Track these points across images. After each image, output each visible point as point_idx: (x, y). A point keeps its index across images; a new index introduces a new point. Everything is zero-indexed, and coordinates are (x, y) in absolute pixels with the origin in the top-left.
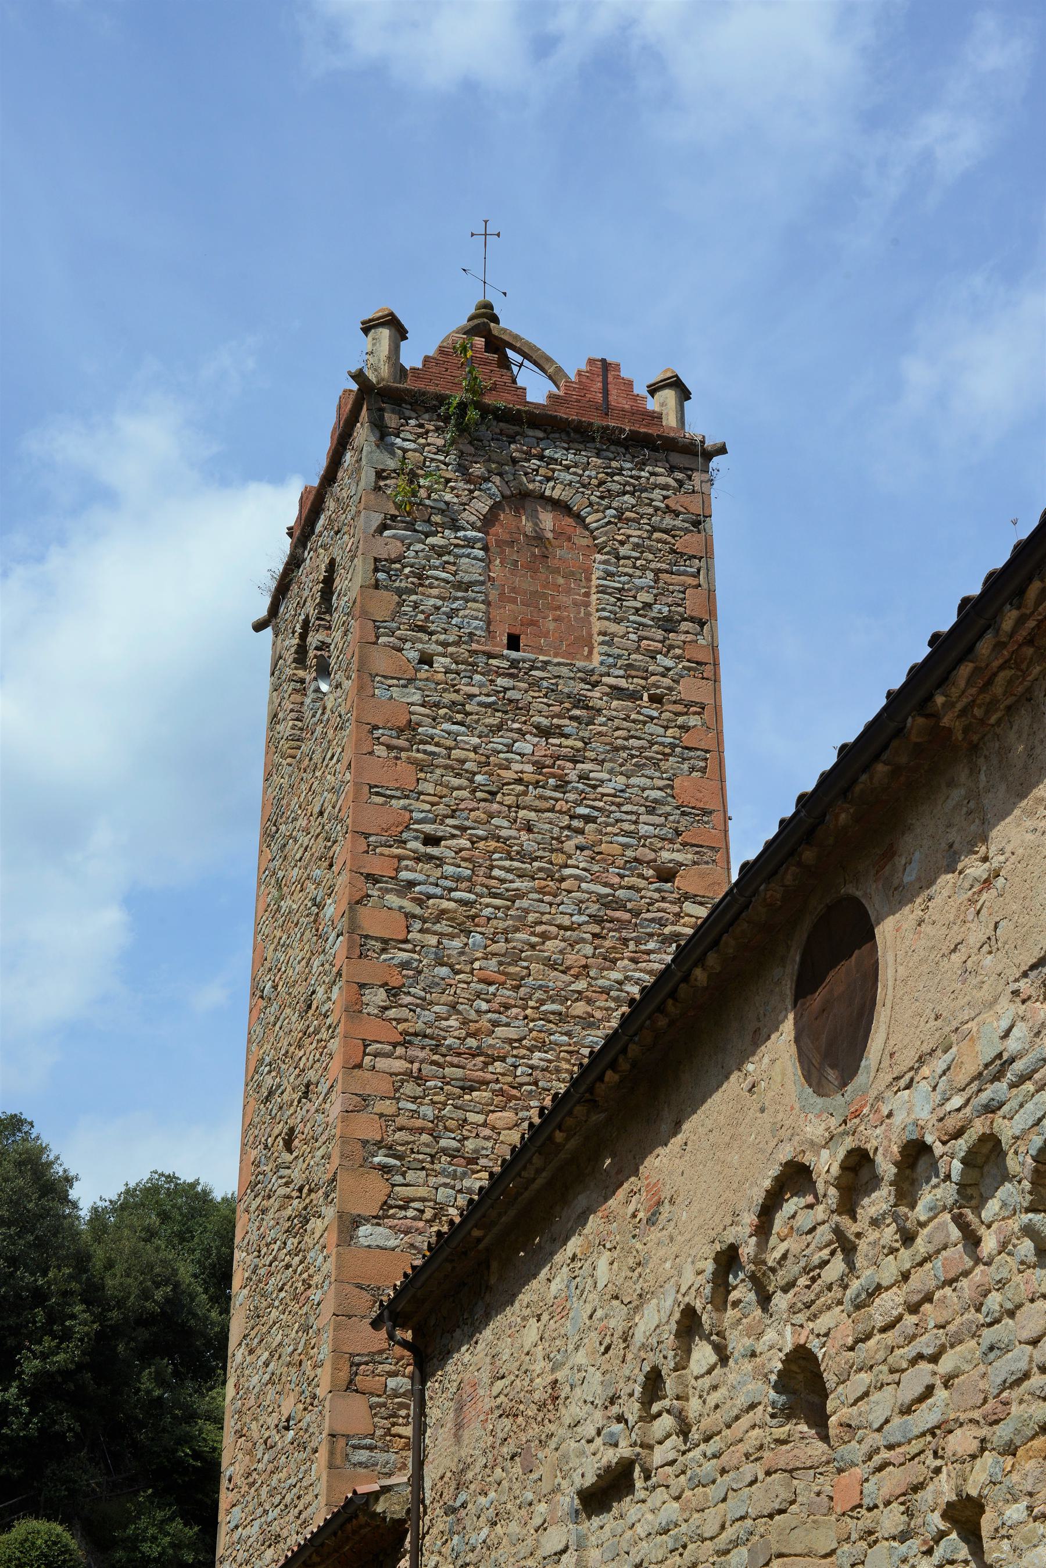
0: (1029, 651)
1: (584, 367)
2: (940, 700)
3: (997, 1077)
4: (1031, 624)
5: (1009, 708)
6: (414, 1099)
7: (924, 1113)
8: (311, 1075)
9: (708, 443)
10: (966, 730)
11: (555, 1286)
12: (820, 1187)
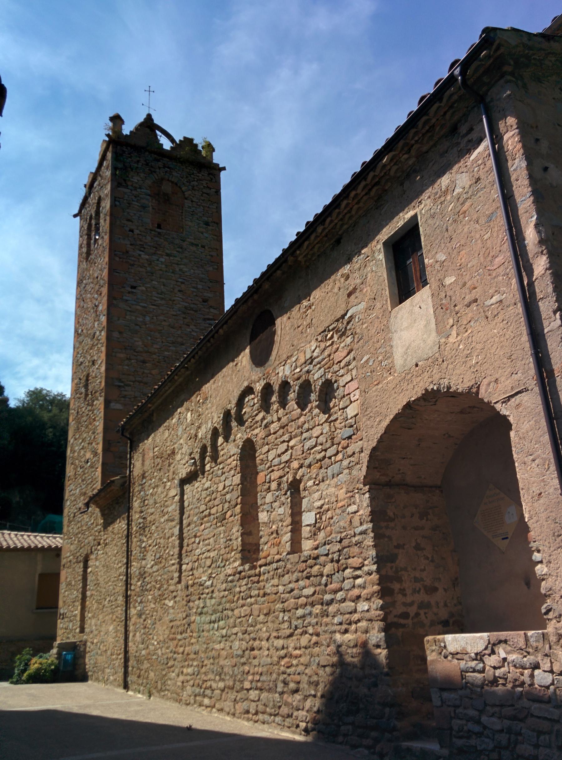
0: (326, 239)
1: (182, 139)
2: (298, 252)
3: (311, 363)
4: (327, 230)
5: (319, 256)
6: (128, 365)
7: (287, 373)
8: (95, 358)
9: (221, 166)
10: (305, 261)
11: (174, 421)
12: (256, 393)
